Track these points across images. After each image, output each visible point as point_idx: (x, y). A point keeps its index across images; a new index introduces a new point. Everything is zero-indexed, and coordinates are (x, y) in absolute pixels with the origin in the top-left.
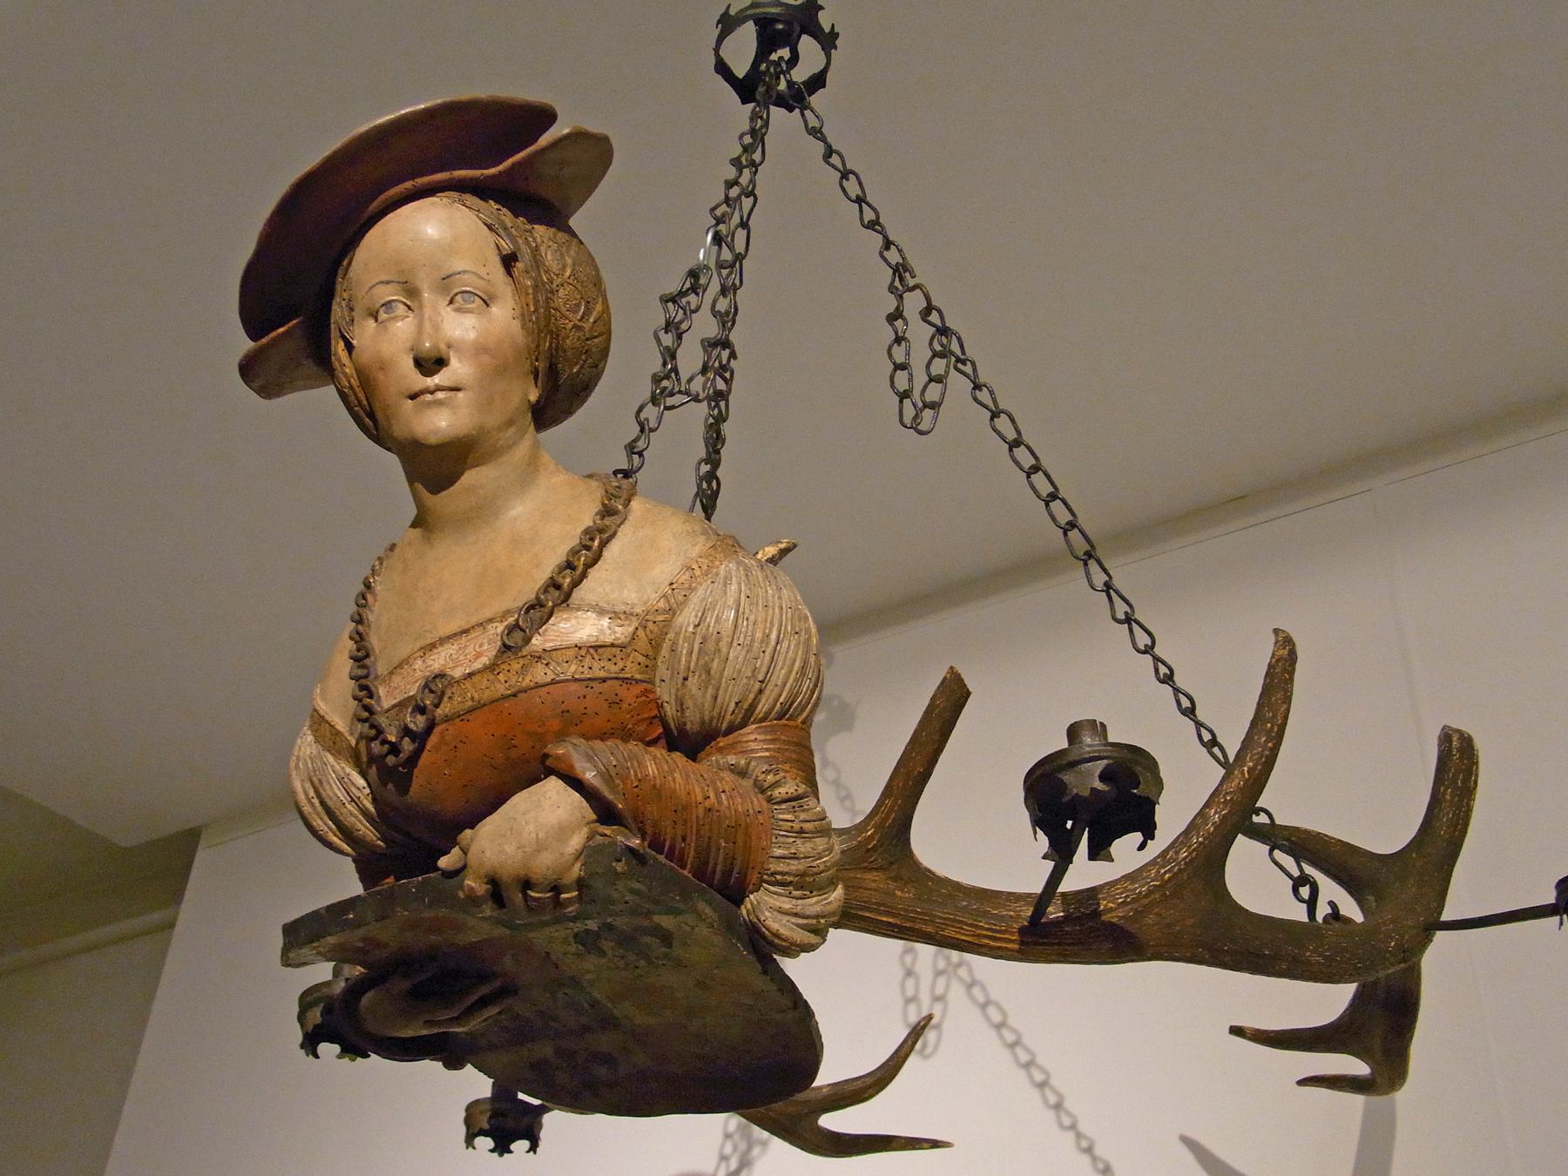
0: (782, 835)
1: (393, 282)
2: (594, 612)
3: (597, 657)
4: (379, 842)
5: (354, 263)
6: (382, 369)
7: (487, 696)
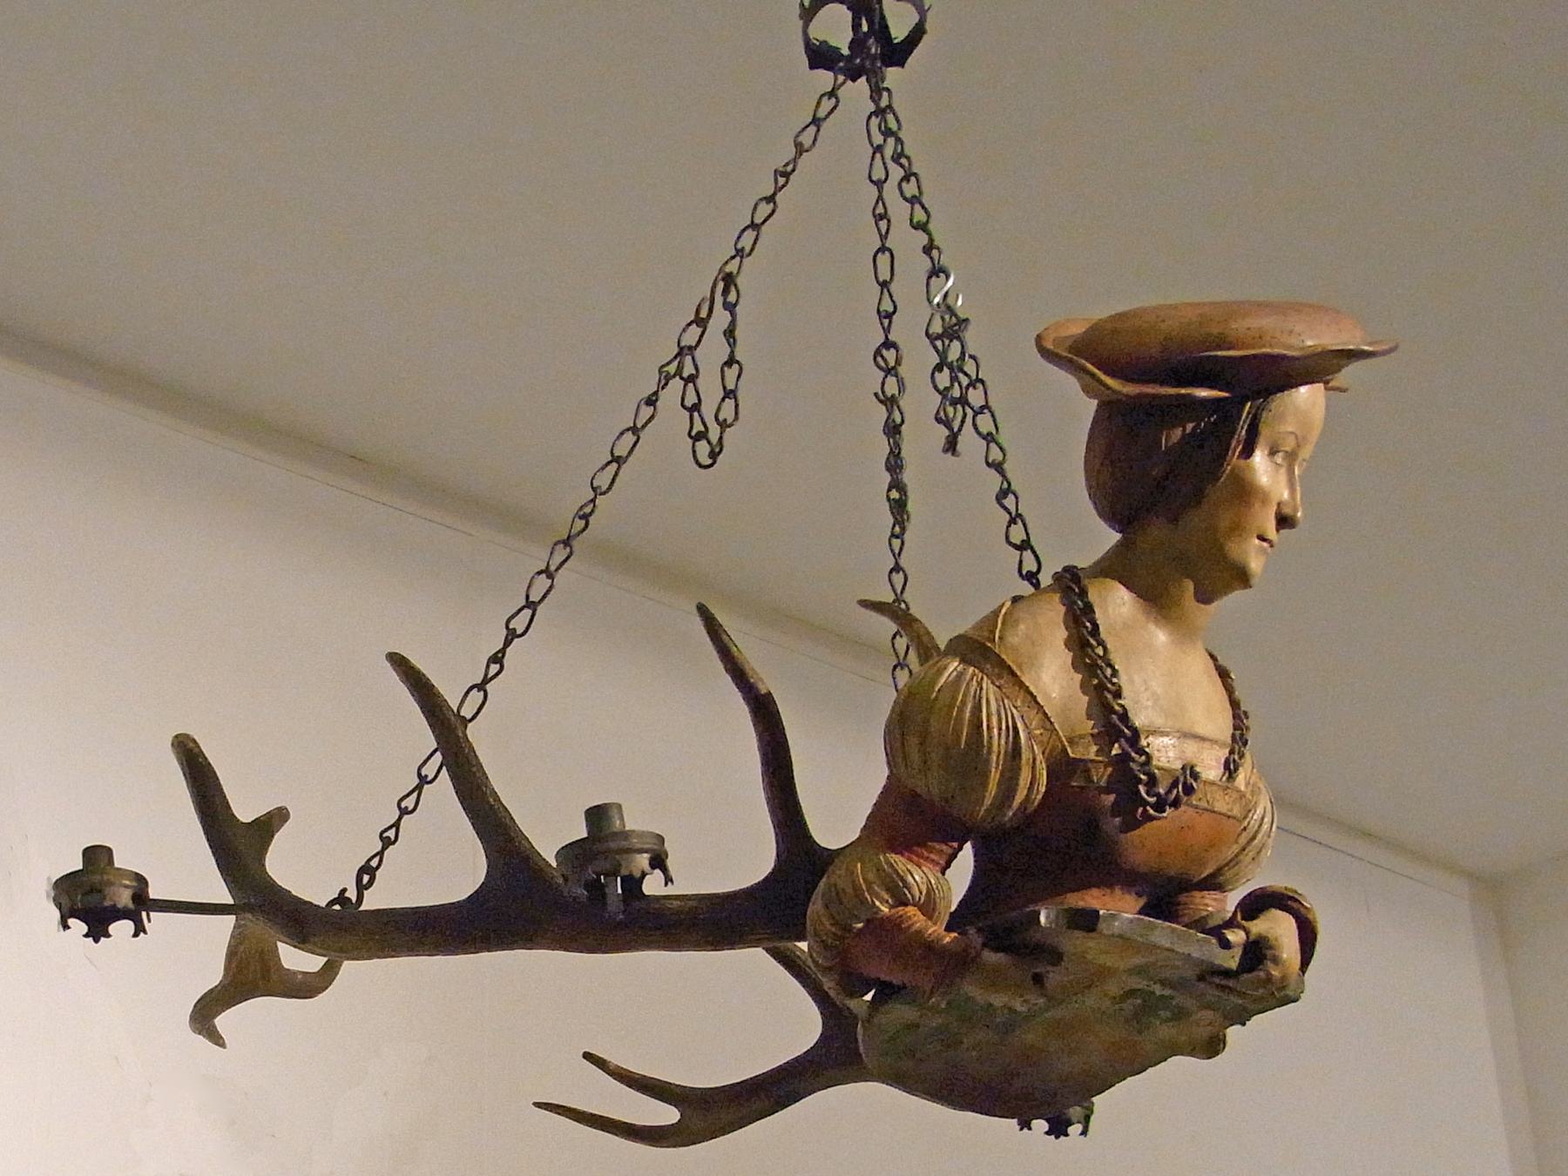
6: (1263, 502)
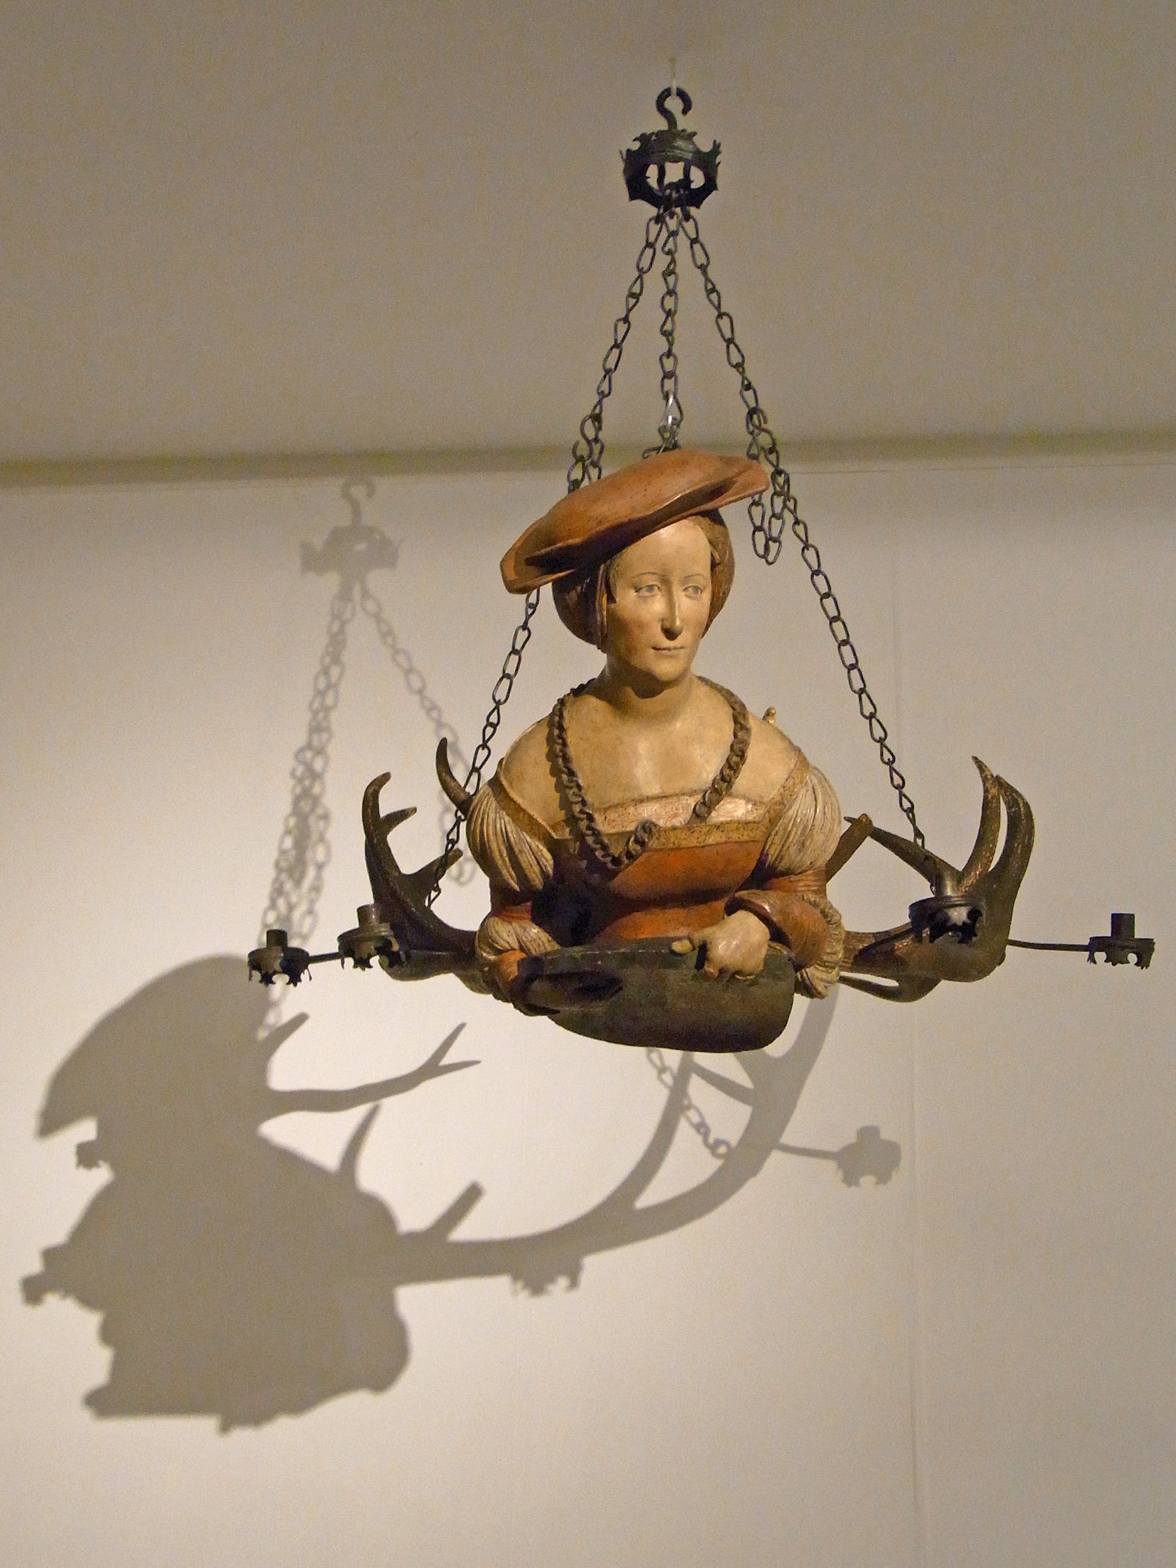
7: (684, 843)
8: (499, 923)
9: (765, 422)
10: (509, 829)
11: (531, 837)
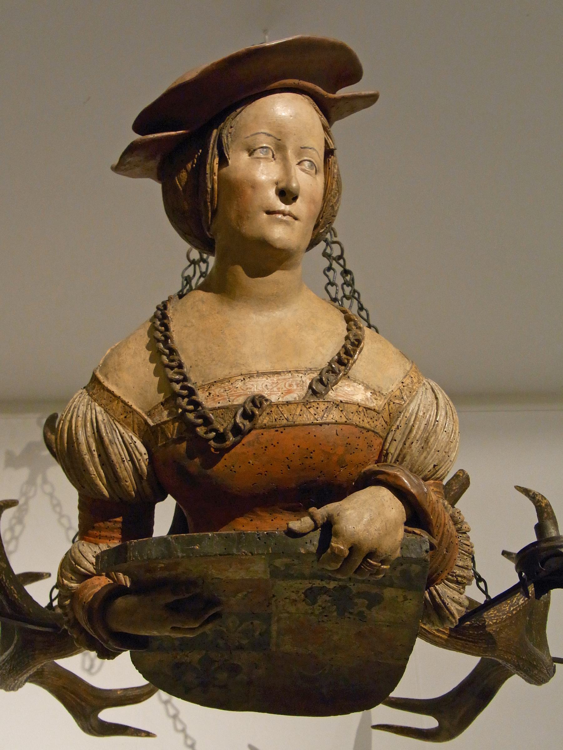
0: (462, 553)
1: (272, 136)
2: (363, 386)
3: (366, 415)
4: (133, 493)
5: (243, 112)
8: (85, 545)
9: (336, 236)
10: (100, 418)
11: (124, 427)
